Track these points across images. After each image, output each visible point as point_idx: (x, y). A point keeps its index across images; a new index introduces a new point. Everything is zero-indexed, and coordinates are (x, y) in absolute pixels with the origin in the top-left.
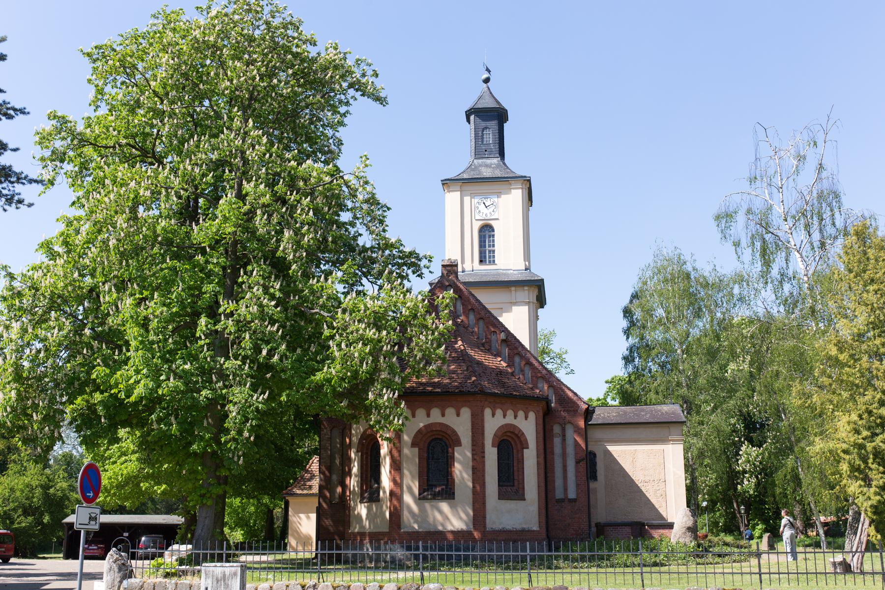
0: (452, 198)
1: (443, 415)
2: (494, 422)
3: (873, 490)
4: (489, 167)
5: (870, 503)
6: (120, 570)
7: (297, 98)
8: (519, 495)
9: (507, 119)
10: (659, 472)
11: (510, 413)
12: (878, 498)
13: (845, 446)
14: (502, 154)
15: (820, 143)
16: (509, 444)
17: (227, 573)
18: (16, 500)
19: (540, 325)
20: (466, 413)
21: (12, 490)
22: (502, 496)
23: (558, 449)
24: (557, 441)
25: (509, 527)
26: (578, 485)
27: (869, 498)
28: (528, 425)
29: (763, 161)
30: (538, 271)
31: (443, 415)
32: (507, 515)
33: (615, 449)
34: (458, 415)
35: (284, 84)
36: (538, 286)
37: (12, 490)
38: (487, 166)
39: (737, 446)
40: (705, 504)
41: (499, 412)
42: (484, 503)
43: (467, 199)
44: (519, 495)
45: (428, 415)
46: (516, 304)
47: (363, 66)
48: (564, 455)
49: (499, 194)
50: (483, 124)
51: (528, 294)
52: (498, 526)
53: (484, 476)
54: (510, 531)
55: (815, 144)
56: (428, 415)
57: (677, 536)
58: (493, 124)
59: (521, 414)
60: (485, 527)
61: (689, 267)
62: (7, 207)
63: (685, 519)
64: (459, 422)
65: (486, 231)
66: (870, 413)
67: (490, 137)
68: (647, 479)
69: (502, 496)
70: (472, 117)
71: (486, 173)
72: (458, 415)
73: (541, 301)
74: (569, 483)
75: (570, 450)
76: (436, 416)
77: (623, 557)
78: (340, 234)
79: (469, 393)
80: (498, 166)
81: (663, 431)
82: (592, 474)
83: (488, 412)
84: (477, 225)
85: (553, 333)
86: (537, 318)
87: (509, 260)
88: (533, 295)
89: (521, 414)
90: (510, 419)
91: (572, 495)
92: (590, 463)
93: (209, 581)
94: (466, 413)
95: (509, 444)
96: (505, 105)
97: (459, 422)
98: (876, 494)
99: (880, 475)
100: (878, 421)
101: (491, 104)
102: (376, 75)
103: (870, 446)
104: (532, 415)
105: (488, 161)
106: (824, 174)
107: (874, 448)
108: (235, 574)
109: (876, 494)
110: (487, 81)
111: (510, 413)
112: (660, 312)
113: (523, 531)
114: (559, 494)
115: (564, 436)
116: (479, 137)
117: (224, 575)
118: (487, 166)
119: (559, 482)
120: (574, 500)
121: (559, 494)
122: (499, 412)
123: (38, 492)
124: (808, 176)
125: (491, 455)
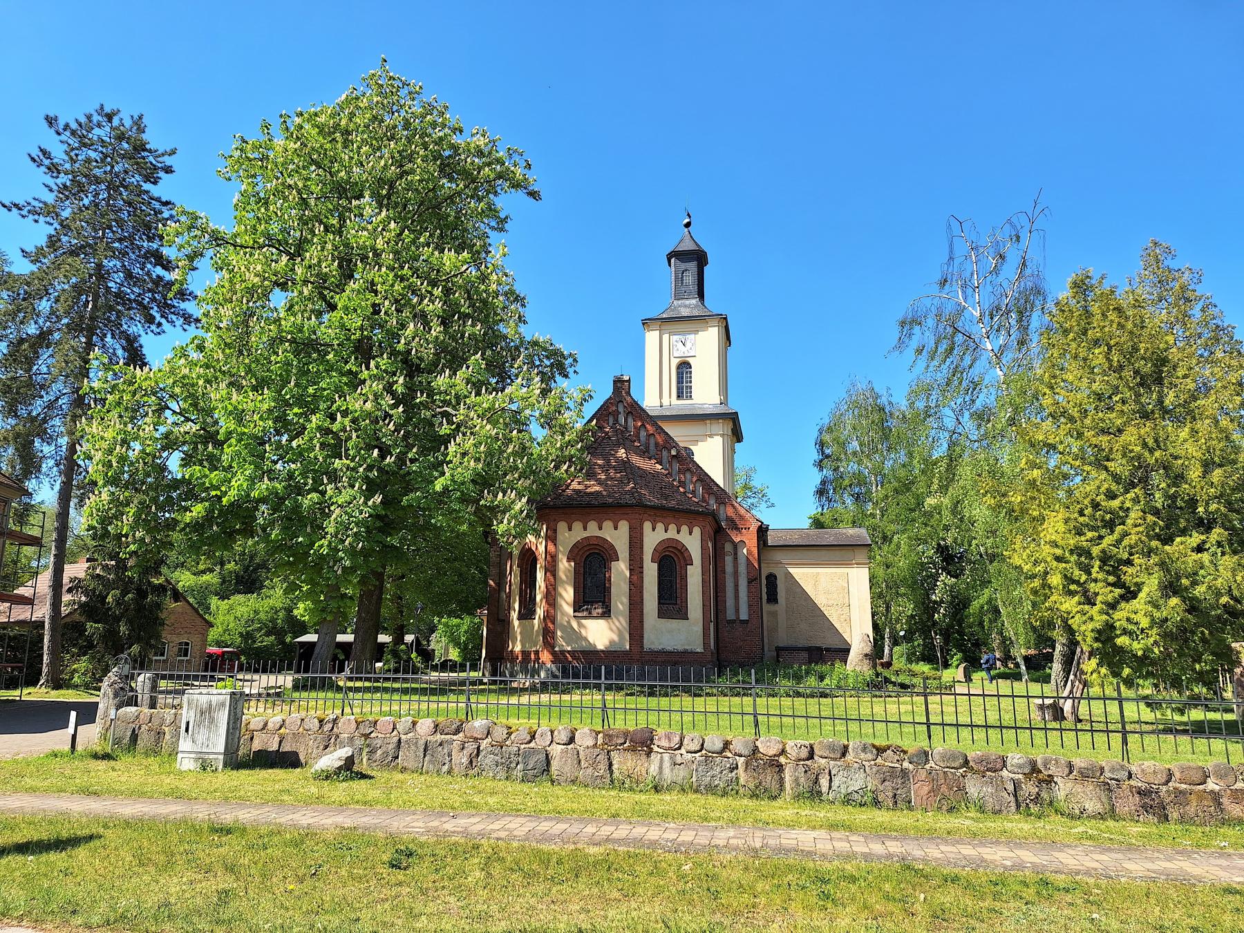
0: (652, 337)
1: (600, 528)
2: (653, 536)
3: (1096, 608)
4: (689, 306)
5: (1090, 626)
6: (116, 695)
7: (444, 196)
8: (682, 614)
9: (707, 263)
10: (843, 597)
11: (672, 527)
12: (1105, 617)
13: (1058, 552)
14: (701, 295)
15: (1024, 235)
16: (671, 561)
17: (214, 704)
18: (260, 621)
19: (739, 462)
20: (624, 526)
21: (256, 612)
22: (662, 615)
23: (729, 568)
24: (729, 560)
25: (669, 648)
26: (750, 606)
27: (1091, 619)
28: (692, 541)
29: (957, 262)
30: (733, 407)
31: (600, 528)
32: (666, 635)
33: (798, 573)
34: (616, 528)
35: (420, 169)
36: (733, 418)
37: (256, 612)
38: (686, 306)
39: (935, 577)
40: (902, 633)
41: (660, 526)
42: (642, 622)
43: (665, 337)
44: (682, 614)
45: (585, 529)
46: (711, 436)
47: (516, 158)
48: (736, 573)
49: (696, 332)
50: (683, 266)
51: (724, 427)
52: (657, 646)
53: (642, 592)
54: (678, 653)
55: (1018, 238)
56: (585, 529)
57: (856, 664)
58: (692, 266)
59: (685, 528)
60: (642, 647)
61: (883, 401)
62: (186, 327)
63: (862, 645)
64: (617, 535)
65: (684, 368)
66: (1096, 506)
67: (690, 279)
68: (830, 603)
69: (662, 615)
70: (673, 260)
71: (685, 312)
72: (616, 528)
73: (737, 435)
74: (740, 605)
75: (742, 569)
76: (593, 530)
77: (785, 684)
78: (480, 333)
79: (627, 506)
80: (696, 306)
81: (847, 553)
82: (773, 598)
83: (647, 526)
84: (675, 362)
85: (753, 469)
86: (733, 451)
87: (706, 394)
88: (727, 428)
89: (685, 528)
90: (672, 533)
91: (744, 616)
92: (769, 587)
93: (192, 713)
94: (624, 526)
95: (671, 561)
96: (705, 247)
97: (617, 535)
98: (1101, 612)
99: (1110, 588)
100: (1108, 517)
101: (692, 247)
102: (529, 166)
103: (1096, 551)
104: (697, 531)
105: (687, 302)
106: (1028, 272)
107: (1103, 551)
108: (223, 704)
109: (1101, 612)
110: (688, 225)
111: (672, 527)
112: (855, 445)
113: (685, 653)
114: (730, 615)
115: (736, 554)
116: (679, 279)
117: (210, 705)
118: (686, 306)
119: (730, 603)
120: (745, 622)
121: (730, 615)
122: (660, 526)
123: (282, 614)
124: (1010, 270)
125: (651, 571)
